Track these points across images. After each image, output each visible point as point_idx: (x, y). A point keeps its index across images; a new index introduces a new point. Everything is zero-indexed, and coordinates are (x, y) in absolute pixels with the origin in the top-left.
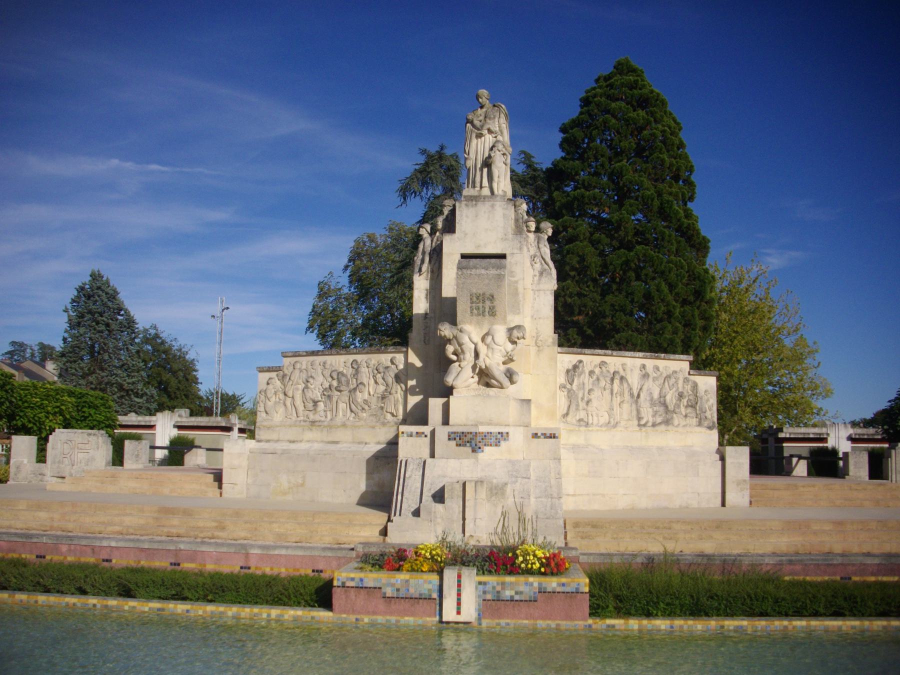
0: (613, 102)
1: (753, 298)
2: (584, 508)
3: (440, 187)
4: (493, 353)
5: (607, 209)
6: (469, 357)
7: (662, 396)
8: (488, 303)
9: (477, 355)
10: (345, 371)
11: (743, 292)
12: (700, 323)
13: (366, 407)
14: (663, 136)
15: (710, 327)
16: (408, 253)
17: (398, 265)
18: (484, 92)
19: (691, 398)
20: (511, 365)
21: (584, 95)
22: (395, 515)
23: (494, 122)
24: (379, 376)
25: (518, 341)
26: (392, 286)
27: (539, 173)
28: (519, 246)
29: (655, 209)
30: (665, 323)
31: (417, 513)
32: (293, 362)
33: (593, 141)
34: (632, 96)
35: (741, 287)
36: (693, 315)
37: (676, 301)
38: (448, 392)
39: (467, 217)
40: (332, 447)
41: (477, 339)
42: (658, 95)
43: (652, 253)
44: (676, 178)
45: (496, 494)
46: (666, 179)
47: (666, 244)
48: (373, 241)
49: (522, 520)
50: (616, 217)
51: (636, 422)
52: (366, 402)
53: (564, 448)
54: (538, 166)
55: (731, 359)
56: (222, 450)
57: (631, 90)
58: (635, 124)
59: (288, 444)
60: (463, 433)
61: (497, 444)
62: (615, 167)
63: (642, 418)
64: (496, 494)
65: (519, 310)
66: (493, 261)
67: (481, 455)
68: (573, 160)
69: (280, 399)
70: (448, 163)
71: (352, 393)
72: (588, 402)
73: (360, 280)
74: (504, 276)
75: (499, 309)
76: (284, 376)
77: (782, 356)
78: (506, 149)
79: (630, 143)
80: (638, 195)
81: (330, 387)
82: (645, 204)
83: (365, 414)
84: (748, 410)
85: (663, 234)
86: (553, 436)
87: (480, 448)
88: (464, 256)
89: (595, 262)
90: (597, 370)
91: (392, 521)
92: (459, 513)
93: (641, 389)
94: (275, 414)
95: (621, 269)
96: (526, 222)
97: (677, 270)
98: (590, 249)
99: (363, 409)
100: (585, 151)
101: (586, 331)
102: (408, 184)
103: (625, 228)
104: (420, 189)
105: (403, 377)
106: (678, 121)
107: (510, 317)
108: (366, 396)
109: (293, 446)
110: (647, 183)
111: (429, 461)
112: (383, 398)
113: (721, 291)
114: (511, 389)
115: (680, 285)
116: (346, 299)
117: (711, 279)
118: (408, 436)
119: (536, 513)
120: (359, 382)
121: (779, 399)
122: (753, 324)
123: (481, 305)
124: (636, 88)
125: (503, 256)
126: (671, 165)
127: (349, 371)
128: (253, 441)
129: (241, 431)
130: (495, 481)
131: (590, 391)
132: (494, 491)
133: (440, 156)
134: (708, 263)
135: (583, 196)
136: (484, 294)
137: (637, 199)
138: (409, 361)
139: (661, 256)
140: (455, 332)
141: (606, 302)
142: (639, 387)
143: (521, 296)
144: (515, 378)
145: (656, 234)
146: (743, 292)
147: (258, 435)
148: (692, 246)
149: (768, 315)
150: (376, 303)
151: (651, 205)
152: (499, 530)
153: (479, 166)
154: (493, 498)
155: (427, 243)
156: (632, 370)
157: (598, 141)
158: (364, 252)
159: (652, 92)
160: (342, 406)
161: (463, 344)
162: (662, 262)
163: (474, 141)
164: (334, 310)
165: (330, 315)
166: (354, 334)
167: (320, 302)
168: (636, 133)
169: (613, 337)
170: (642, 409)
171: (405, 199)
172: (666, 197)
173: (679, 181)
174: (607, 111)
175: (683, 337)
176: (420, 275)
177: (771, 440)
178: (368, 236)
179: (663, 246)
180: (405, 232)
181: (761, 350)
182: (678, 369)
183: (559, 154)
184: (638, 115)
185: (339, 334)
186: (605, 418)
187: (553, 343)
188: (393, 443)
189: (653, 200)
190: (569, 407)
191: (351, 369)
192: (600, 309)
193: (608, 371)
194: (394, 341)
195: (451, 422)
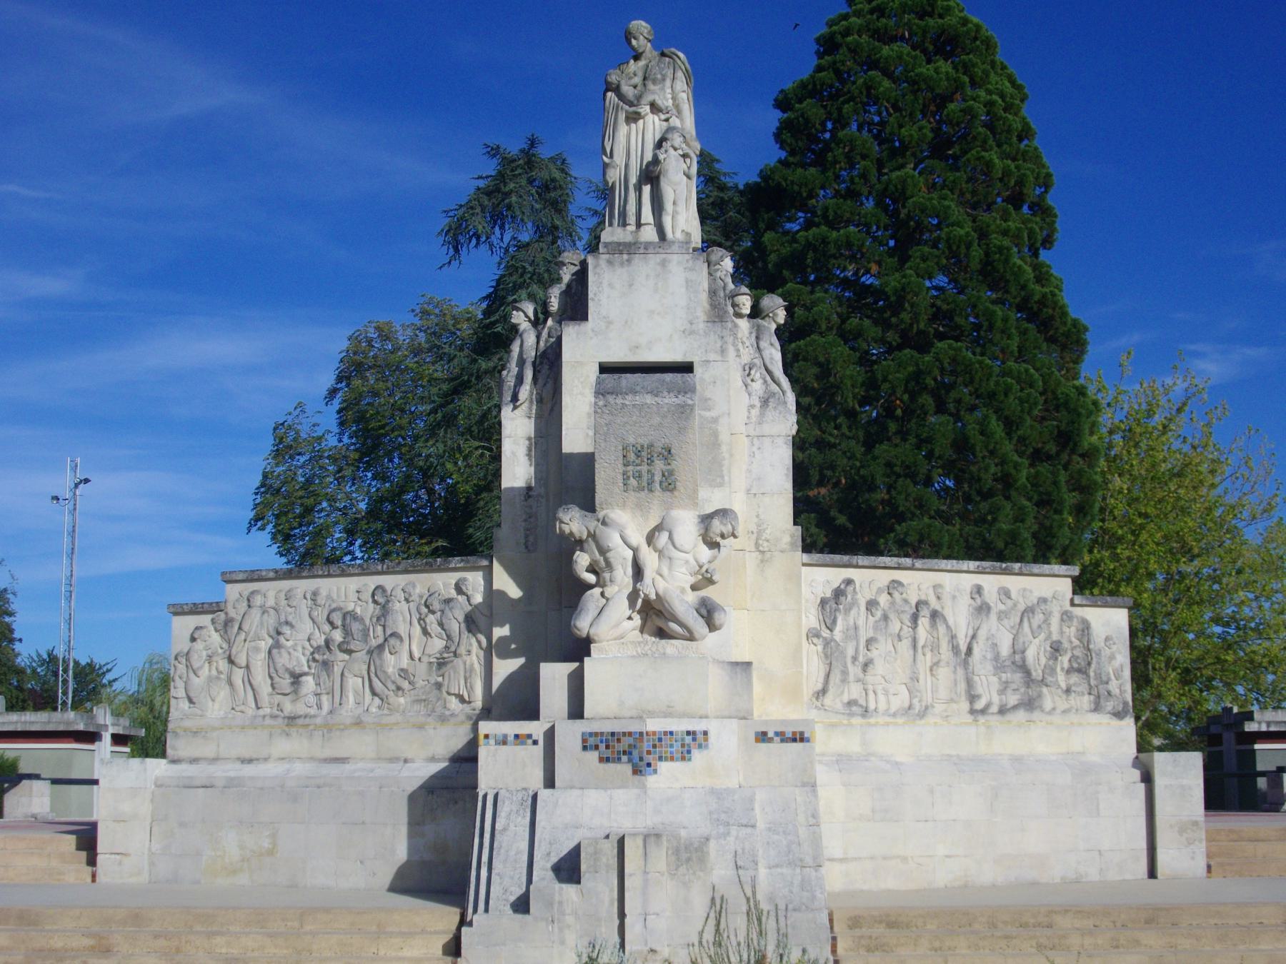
0: (885, 44)
1: (1176, 445)
2: (865, 887)
3: (530, 225)
4: (670, 569)
5: (874, 268)
6: (623, 575)
7: (1018, 649)
8: (659, 465)
9: (638, 572)
10: (358, 610)
11: (1156, 434)
12: (1071, 498)
13: (405, 685)
14: (988, 114)
15: (1091, 507)
16: (465, 362)
17: (445, 387)
18: (641, 27)
19: (1078, 653)
20: (708, 592)
21: (824, 30)
22: (475, 911)
23: (663, 89)
24: (431, 619)
25: (722, 542)
26: (432, 431)
27: (730, 193)
28: (719, 343)
29: (975, 264)
30: (997, 499)
31: (522, 905)
32: (246, 594)
33: (843, 127)
34: (925, 32)
35: (1153, 424)
36: (1055, 483)
37: (1021, 454)
38: (579, 649)
39: (611, 285)
40: (334, 770)
41: (638, 539)
42: (978, 27)
43: (970, 354)
44: (1016, 200)
45: (689, 860)
46: (994, 203)
47: (998, 337)
48: (388, 338)
49: (755, 915)
50: (894, 282)
51: (965, 706)
52: (404, 673)
53: (820, 762)
54: (728, 179)
55: (1135, 570)
56: (96, 782)
57: (921, 18)
58: (931, 89)
59: (238, 765)
60: (613, 734)
61: (685, 756)
62: (890, 181)
63: (979, 697)
64: (689, 860)
65: (722, 477)
66: (668, 377)
67: (651, 780)
68: (804, 166)
69: (220, 672)
70: (544, 175)
71: (375, 655)
72: (866, 666)
73: (361, 418)
74: (692, 407)
75: (682, 477)
76: (228, 622)
77: (1239, 564)
78: (688, 145)
79: (921, 129)
80: (939, 238)
81: (328, 643)
82: (954, 254)
83: (402, 700)
84: (1173, 675)
85: (990, 316)
86: (799, 738)
87: (649, 765)
88: (605, 369)
89: (851, 377)
90: (883, 599)
91: (470, 924)
92: (612, 904)
93: (974, 637)
94: (210, 703)
95: (906, 391)
96: (733, 296)
97: (1022, 390)
98: (841, 351)
99: (399, 688)
100: (827, 148)
101: (834, 519)
102: (462, 218)
103: (912, 306)
104: (488, 229)
105: (482, 621)
106: (1019, 82)
107: (703, 493)
108: (405, 662)
109: (249, 770)
110: (956, 211)
111: (544, 794)
112: (441, 664)
113: (1111, 432)
114: (710, 641)
115: (1029, 421)
116: (334, 459)
117: (1091, 407)
118: (497, 743)
119: (771, 899)
120: (389, 632)
121: (1235, 652)
122: (1179, 499)
123: (644, 468)
124: (931, 15)
125: (687, 368)
126: (1006, 173)
127: (367, 610)
128: (163, 762)
129: (118, 739)
130: (683, 833)
131: (869, 642)
132: (684, 856)
133: (529, 159)
134: (1083, 375)
135: (824, 241)
136: (651, 446)
137: (935, 246)
138: (495, 587)
139: (988, 361)
140: (593, 525)
141: (874, 458)
142: (971, 633)
143: (724, 448)
144: (718, 618)
145: (976, 317)
146: (1156, 434)
147: (174, 748)
148: (1052, 340)
149: (1210, 479)
150: (396, 468)
151: (967, 255)
152: (709, 936)
153: (633, 180)
154: (682, 870)
155: (529, 342)
156: (954, 597)
157: (854, 127)
158: (370, 362)
159: (965, 22)
160: (354, 683)
161: (609, 550)
162: (990, 375)
163: (623, 129)
164: (309, 481)
165: (301, 493)
166: (351, 533)
167: (277, 465)
168: (933, 108)
169: (892, 530)
170: (976, 678)
171: (457, 250)
172: (996, 240)
173: (1021, 207)
174: (873, 64)
175: (1035, 527)
176: (515, 408)
177: (1229, 738)
178: (378, 328)
179: (991, 341)
180: (454, 317)
181: (1196, 551)
182: (1048, 594)
183: (772, 154)
184: (937, 71)
185: (320, 533)
186: (901, 699)
187: (793, 544)
188: (466, 759)
189: (969, 246)
190: (828, 676)
191: (371, 606)
192: (863, 472)
193: (906, 601)
194: (434, 545)
195: (588, 712)
